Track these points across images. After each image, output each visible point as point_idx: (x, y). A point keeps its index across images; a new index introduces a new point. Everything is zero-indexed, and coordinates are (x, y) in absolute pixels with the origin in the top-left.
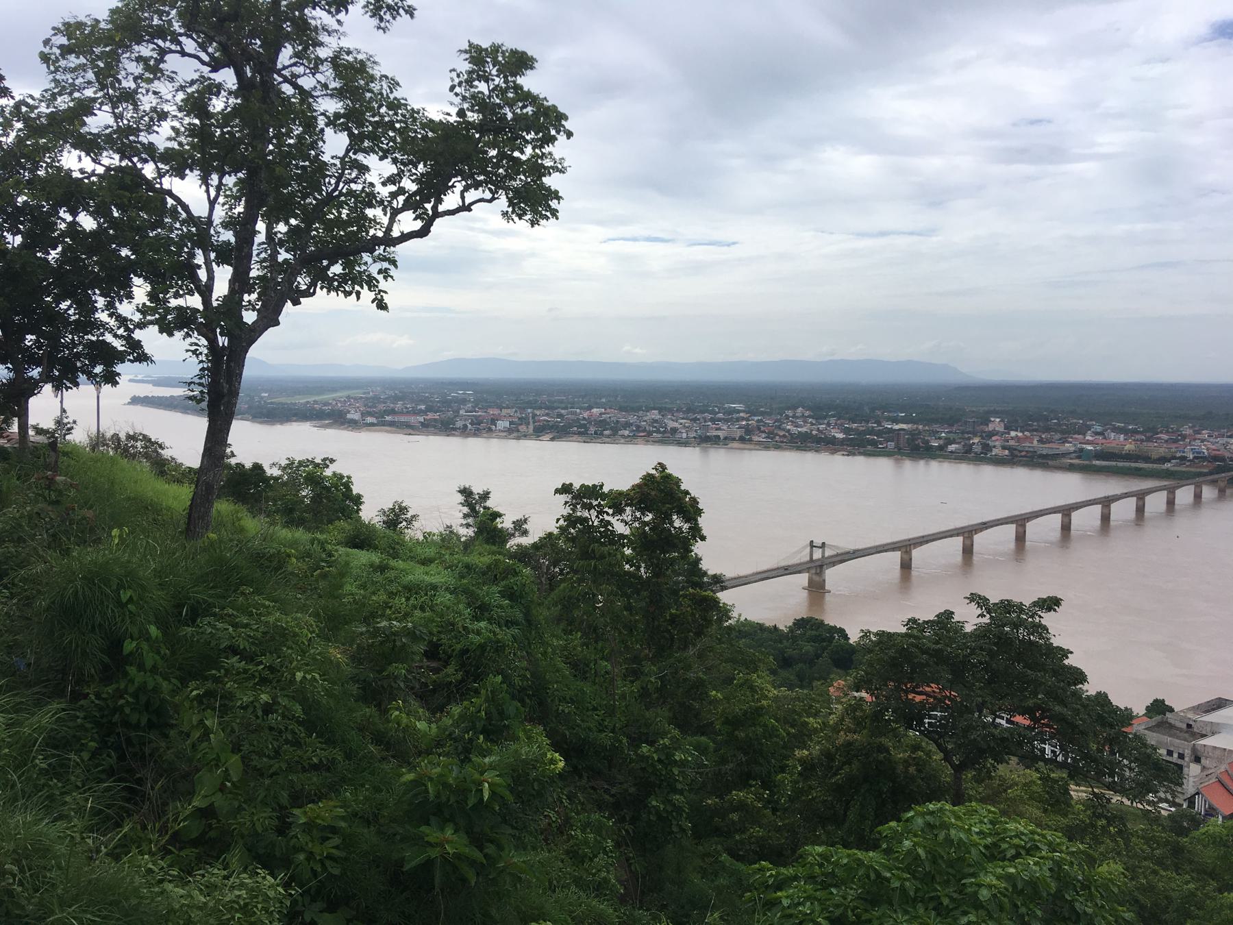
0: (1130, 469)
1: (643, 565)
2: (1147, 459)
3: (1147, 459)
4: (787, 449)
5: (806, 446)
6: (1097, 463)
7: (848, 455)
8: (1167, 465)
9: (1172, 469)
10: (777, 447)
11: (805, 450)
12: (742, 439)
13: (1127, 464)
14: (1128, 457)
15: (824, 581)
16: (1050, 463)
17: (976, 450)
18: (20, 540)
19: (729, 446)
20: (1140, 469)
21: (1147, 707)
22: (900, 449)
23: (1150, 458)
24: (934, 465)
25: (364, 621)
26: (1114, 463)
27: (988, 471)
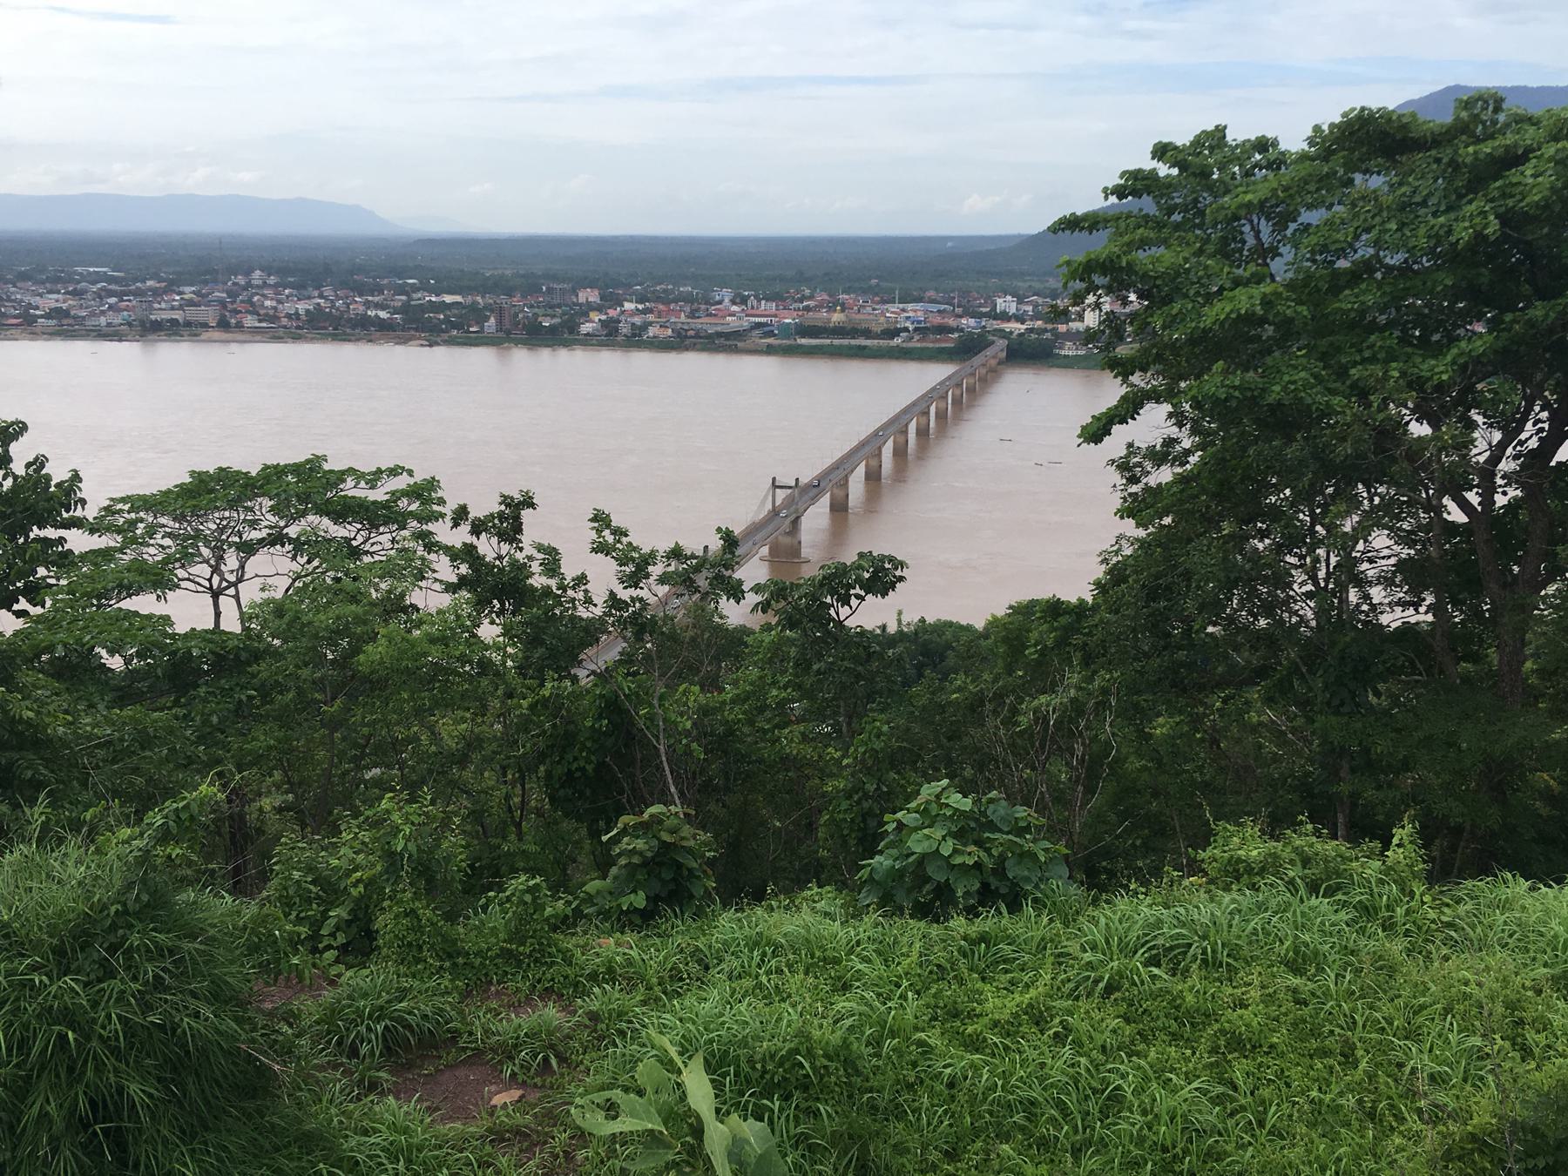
0: (850, 347)
1: (35, 532)
2: (867, 333)
3: (867, 333)
4: (312, 339)
5: (345, 333)
6: (804, 341)
7: (430, 346)
8: (897, 341)
9: (904, 345)
10: (277, 338)
11: (344, 340)
12: (223, 325)
13: (845, 342)
14: (839, 331)
15: (800, 542)
16: (739, 344)
17: (625, 330)
18: (647, 694)
19: (202, 337)
20: (865, 347)
21: (193, 630)
22: (508, 333)
23: (870, 332)
24: (563, 354)
25: (237, 716)
26: (828, 341)
27: (642, 360)
